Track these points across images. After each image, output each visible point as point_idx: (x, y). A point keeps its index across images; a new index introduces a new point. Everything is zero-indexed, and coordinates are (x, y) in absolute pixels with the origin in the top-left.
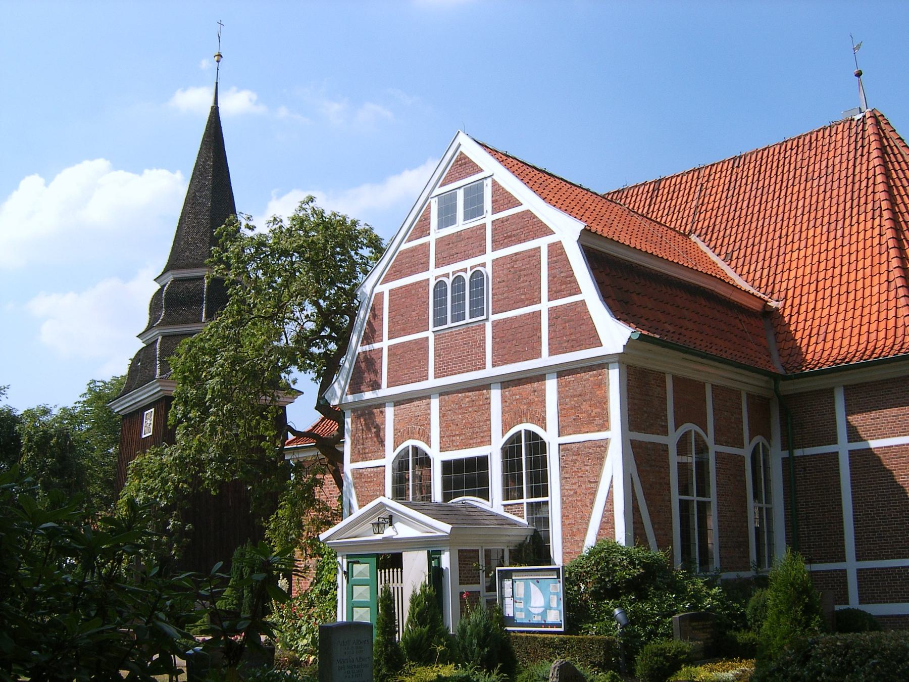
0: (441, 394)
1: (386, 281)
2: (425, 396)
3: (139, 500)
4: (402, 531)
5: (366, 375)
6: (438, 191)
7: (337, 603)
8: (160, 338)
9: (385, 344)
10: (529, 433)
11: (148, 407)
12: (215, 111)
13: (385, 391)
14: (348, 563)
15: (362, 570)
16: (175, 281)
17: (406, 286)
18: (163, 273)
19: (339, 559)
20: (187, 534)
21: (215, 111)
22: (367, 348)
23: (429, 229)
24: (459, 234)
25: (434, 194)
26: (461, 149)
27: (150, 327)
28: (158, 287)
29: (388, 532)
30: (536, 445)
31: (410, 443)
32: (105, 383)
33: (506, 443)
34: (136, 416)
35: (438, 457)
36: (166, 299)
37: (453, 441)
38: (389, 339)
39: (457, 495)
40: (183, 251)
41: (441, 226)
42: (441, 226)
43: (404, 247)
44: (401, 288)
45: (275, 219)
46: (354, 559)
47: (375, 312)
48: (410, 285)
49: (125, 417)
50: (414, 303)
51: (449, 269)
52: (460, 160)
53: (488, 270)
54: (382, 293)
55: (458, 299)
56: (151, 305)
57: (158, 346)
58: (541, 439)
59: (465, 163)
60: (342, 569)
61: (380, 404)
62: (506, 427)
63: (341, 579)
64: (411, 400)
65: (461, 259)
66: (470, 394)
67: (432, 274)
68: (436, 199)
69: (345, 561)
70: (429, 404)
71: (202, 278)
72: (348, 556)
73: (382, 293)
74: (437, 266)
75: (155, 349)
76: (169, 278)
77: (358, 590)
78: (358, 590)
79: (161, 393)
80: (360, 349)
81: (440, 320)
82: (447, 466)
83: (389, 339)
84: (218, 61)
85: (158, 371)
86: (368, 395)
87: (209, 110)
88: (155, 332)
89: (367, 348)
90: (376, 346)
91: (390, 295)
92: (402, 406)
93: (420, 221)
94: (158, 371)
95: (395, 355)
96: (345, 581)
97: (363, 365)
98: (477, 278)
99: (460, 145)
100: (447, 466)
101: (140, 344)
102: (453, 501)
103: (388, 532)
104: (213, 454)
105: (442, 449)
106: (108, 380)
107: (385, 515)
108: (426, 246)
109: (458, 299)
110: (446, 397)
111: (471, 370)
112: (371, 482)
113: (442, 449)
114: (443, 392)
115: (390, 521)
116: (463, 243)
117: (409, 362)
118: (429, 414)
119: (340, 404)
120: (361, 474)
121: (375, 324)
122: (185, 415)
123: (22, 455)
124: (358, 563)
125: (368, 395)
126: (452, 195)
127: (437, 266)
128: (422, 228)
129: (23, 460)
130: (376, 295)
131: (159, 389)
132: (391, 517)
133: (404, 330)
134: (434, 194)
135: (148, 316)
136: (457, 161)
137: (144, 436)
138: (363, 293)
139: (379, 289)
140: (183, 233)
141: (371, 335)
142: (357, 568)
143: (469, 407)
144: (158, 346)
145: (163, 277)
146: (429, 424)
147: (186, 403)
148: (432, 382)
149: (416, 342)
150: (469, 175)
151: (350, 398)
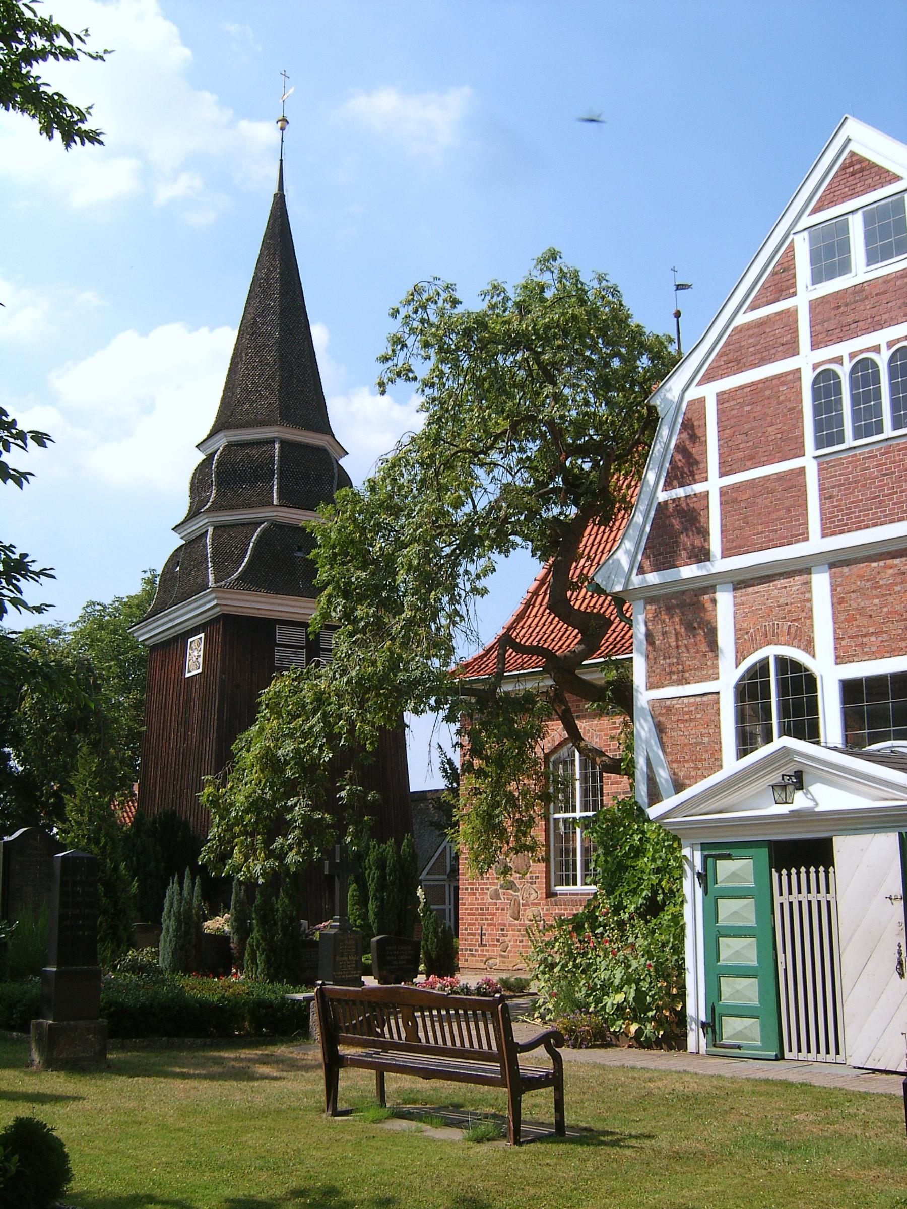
0: (832, 565)
1: (709, 378)
2: (801, 569)
3: (287, 749)
4: (825, 797)
5: (683, 538)
6: (807, 221)
7: (683, 928)
8: (210, 530)
9: (713, 484)
10: (784, 663)
11: (194, 631)
12: (280, 203)
13: (720, 564)
14: (705, 859)
15: (735, 870)
16: (230, 446)
17: (752, 384)
18: (210, 436)
19: (686, 852)
20: (372, 808)
21: (280, 203)
22: (680, 492)
23: (794, 285)
24: (858, 289)
25: (799, 227)
26: (852, 147)
27: (193, 514)
28: (201, 457)
29: (800, 801)
30: (796, 681)
31: (770, 652)
32: (105, 607)
33: (742, 678)
34: (176, 644)
35: (829, 675)
36: (217, 474)
37: (862, 645)
38: (722, 475)
39: (885, 737)
40: (240, 403)
41: (817, 278)
42: (817, 278)
43: (742, 319)
44: (742, 388)
45: (495, 287)
46: (716, 851)
47: (692, 429)
48: (760, 382)
49: (153, 648)
50: (770, 411)
51: (843, 349)
52: (851, 165)
53: (844, 372)
54: (702, 401)
55: (866, 398)
56: (192, 484)
57: (209, 540)
58: (806, 670)
59: (862, 170)
60: (693, 868)
61: (706, 587)
62: (740, 657)
63: (690, 887)
64: (768, 579)
65: (867, 331)
66: (897, 561)
67: (806, 361)
68: (806, 234)
69: (698, 855)
70: (808, 583)
71: (271, 442)
72: (704, 846)
73: (702, 401)
74: (815, 345)
75: (205, 546)
76: (221, 442)
77: (727, 907)
78: (727, 907)
79: (218, 609)
80: (662, 496)
81: (828, 433)
82: (851, 690)
83: (722, 475)
84: (282, 129)
85: (211, 577)
86: (688, 571)
87: (270, 201)
88: (201, 521)
89: (680, 492)
90: (698, 488)
91: (719, 402)
92: (750, 590)
93: (774, 273)
94: (211, 577)
95: (735, 501)
96: (699, 891)
97: (676, 524)
98: (865, 371)
99: (848, 140)
100: (851, 690)
101: (177, 541)
102: (868, 748)
103: (800, 801)
104: (418, 673)
105: (840, 660)
106: (107, 601)
107: (790, 769)
108: (790, 315)
109: (866, 398)
110: (845, 570)
111: (867, 527)
112: (691, 720)
113: (840, 660)
114: (836, 562)
115: (798, 781)
116: (868, 304)
117: (767, 512)
118: (810, 600)
119: (625, 590)
120: (669, 709)
121: (694, 451)
122: (347, 615)
123: (23, 699)
124: (728, 857)
125: (688, 571)
126: (840, 227)
127: (815, 345)
128: (781, 283)
129: (26, 704)
130: (690, 404)
131: (214, 603)
132: (799, 775)
133: (751, 458)
134: (799, 227)
135: (187, 500)
136: (843, 168)
137: (187, 675)
138: (665, 400)
139: (694, 393)
140: (239, 376)
141: (686, 467)
142: (725, 868)
143: (895, 584)
144: (209, 540)
145: (210, 442)
146: (811, 617)
147: (346, 595)
148: (817, 543)
149: (780, 477)
150: (873, 188)
151: (653, 578)
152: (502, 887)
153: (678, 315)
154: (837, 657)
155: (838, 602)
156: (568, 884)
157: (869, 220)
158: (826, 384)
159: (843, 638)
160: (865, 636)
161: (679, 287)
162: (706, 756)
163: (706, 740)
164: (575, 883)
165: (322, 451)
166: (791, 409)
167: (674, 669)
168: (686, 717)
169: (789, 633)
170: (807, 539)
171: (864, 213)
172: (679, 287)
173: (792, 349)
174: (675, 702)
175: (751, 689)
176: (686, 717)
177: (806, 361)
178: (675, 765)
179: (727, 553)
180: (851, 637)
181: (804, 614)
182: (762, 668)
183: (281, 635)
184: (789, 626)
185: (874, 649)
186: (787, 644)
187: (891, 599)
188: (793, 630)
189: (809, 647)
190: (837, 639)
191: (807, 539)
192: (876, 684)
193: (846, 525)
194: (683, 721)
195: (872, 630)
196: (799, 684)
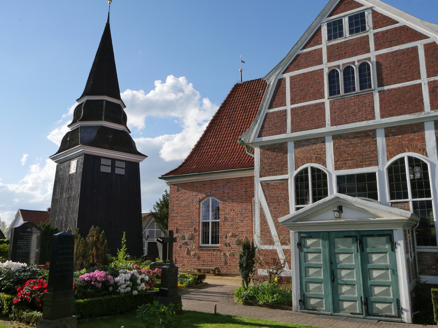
9: (289, 107)
27: (74, 122)
31: (308, 165)
38: (292, 104)
51: (341, 62)
81: (333, 91)
100: (339, 178)
112: (277, 188)
113: (337, 168)
117: (309, 117)
126: (340, 22)
143: (359, 143)
148: (329, 128)
149: (315, 105)
152: (183, 244)
153: (241, 71)
154: (335, 168)
155: (336, 149)
156: (206, 244)
157: (350, 19)
158: (333, 74)
159: (338, 161)
160: (346, 160)
161: (242, 61)
162: (283, 201)
163: (283, 195)
164: (208, 243)
165: (119, 105)
166: (319, 82)
167: (271, 170)
168: (275, 187)
169: (316, 159)
170: (325, 127)
171: (349, 17)
172: (242, 61)
173: (320, 62)
174: (270, 182)
175: (301, 179)
176: (275, 187)
177: (326, 66)
178: (271, 204)
179: (293, 131)
180: (341, 161)
181: (322, 153)
182: (306, 170)
183: (103, 161)
184: (316, 157)
185: (350, 165)
186: (315, 162)
187: (357, 148)
188: (318, 158)
189: (324, 163)
190: (336, 162)
191: (325, 127)
192: (350, 177)
193: (340, 122)
194: (274, 189)
195: (349, 158)
196: (320, 178)
